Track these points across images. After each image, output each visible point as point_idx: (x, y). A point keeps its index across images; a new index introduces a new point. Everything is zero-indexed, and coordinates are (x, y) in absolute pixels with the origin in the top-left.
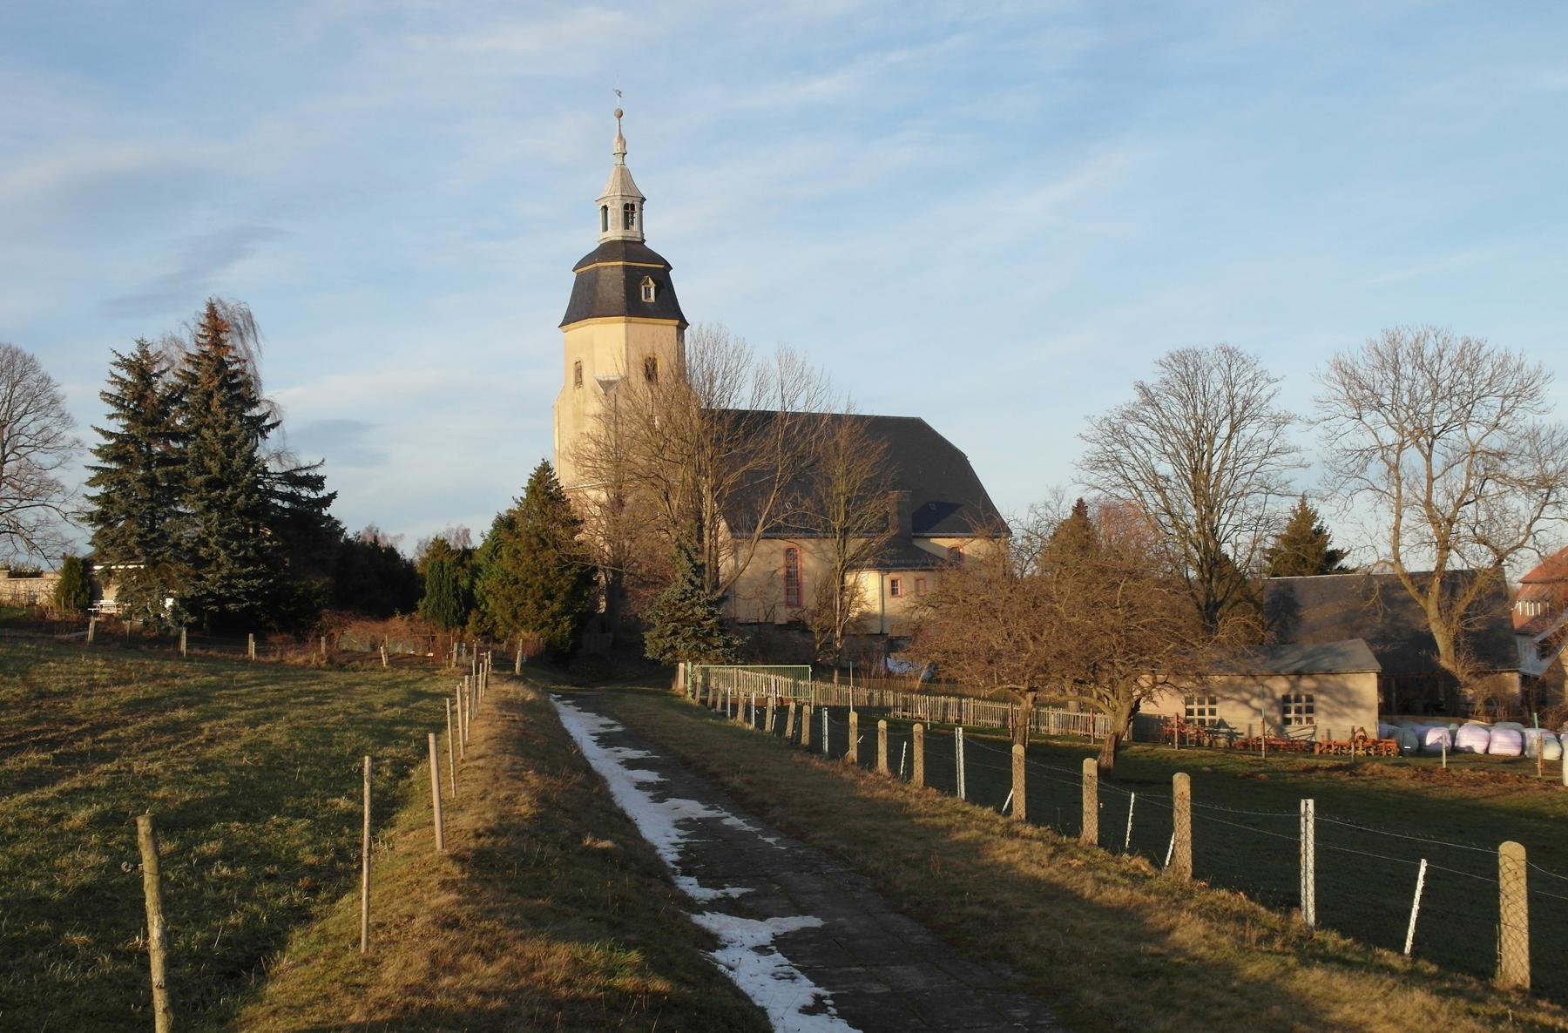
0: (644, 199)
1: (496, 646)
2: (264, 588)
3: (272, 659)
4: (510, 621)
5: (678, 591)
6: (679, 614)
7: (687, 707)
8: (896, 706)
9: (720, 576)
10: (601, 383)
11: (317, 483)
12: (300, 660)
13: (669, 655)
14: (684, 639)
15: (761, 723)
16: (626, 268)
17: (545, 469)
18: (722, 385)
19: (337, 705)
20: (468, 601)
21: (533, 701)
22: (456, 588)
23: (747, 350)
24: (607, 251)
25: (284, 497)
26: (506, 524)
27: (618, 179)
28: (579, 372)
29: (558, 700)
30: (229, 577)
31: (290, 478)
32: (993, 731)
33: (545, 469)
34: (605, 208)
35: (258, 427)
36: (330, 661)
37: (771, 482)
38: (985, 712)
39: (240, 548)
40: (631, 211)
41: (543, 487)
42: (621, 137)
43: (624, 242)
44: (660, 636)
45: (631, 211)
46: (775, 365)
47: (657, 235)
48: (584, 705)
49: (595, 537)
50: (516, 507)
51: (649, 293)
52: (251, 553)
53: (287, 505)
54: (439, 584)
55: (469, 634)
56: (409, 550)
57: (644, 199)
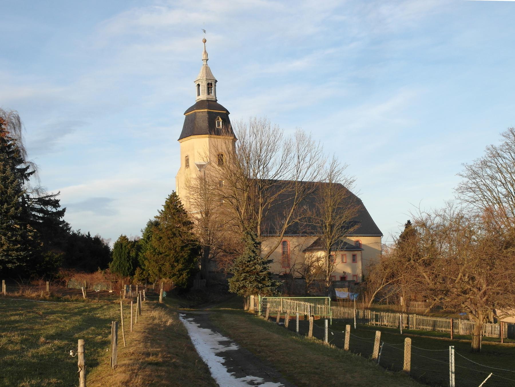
0: (216, 81)
1: (149, 286)
2: (27, 257)
3: (16, 294)
4: (158, 273)
5: (247, 256)
6: (248, 268)
7: (262, 323)
8: (372, 319)
9: (245, 255)
10: (198, 165)
11: (56, 204)
12: (34, 295)
13: (242, 291)
14: (250, 282)
15: (337, 339)
17: (174, 196)
18: (267, 149)
20: (136, 264)
21: (172, 325)
22: (129, 257)
23: (281, 130)
24: (200, 105)
25: (41, 211)
26: (153, 226)
27: (205, 71)
28: (187, 161)
29: (184, 318)
30: (8, 250)
31: (42, 201)
32: (428, 333)
33: (174, 196)
34: (199, 85)
35: (23, 175)
36: (52, 295)
37: (292, 201)
38: (423, 322)
39: (13, 235)
40: (210, 86)
41: (173, 204)
42: (205, 52)
43: (208, 101)
44: (237, 281)
45: (210, 86)
46: (294, 140)
48: (203, 323)
49: (197, 231)
50: (158, 215)
51: (220, 123)
52: (19, 238)
53: (41, 215)
54: (120, 255)
55: (135, 280)
57: (216, 81)
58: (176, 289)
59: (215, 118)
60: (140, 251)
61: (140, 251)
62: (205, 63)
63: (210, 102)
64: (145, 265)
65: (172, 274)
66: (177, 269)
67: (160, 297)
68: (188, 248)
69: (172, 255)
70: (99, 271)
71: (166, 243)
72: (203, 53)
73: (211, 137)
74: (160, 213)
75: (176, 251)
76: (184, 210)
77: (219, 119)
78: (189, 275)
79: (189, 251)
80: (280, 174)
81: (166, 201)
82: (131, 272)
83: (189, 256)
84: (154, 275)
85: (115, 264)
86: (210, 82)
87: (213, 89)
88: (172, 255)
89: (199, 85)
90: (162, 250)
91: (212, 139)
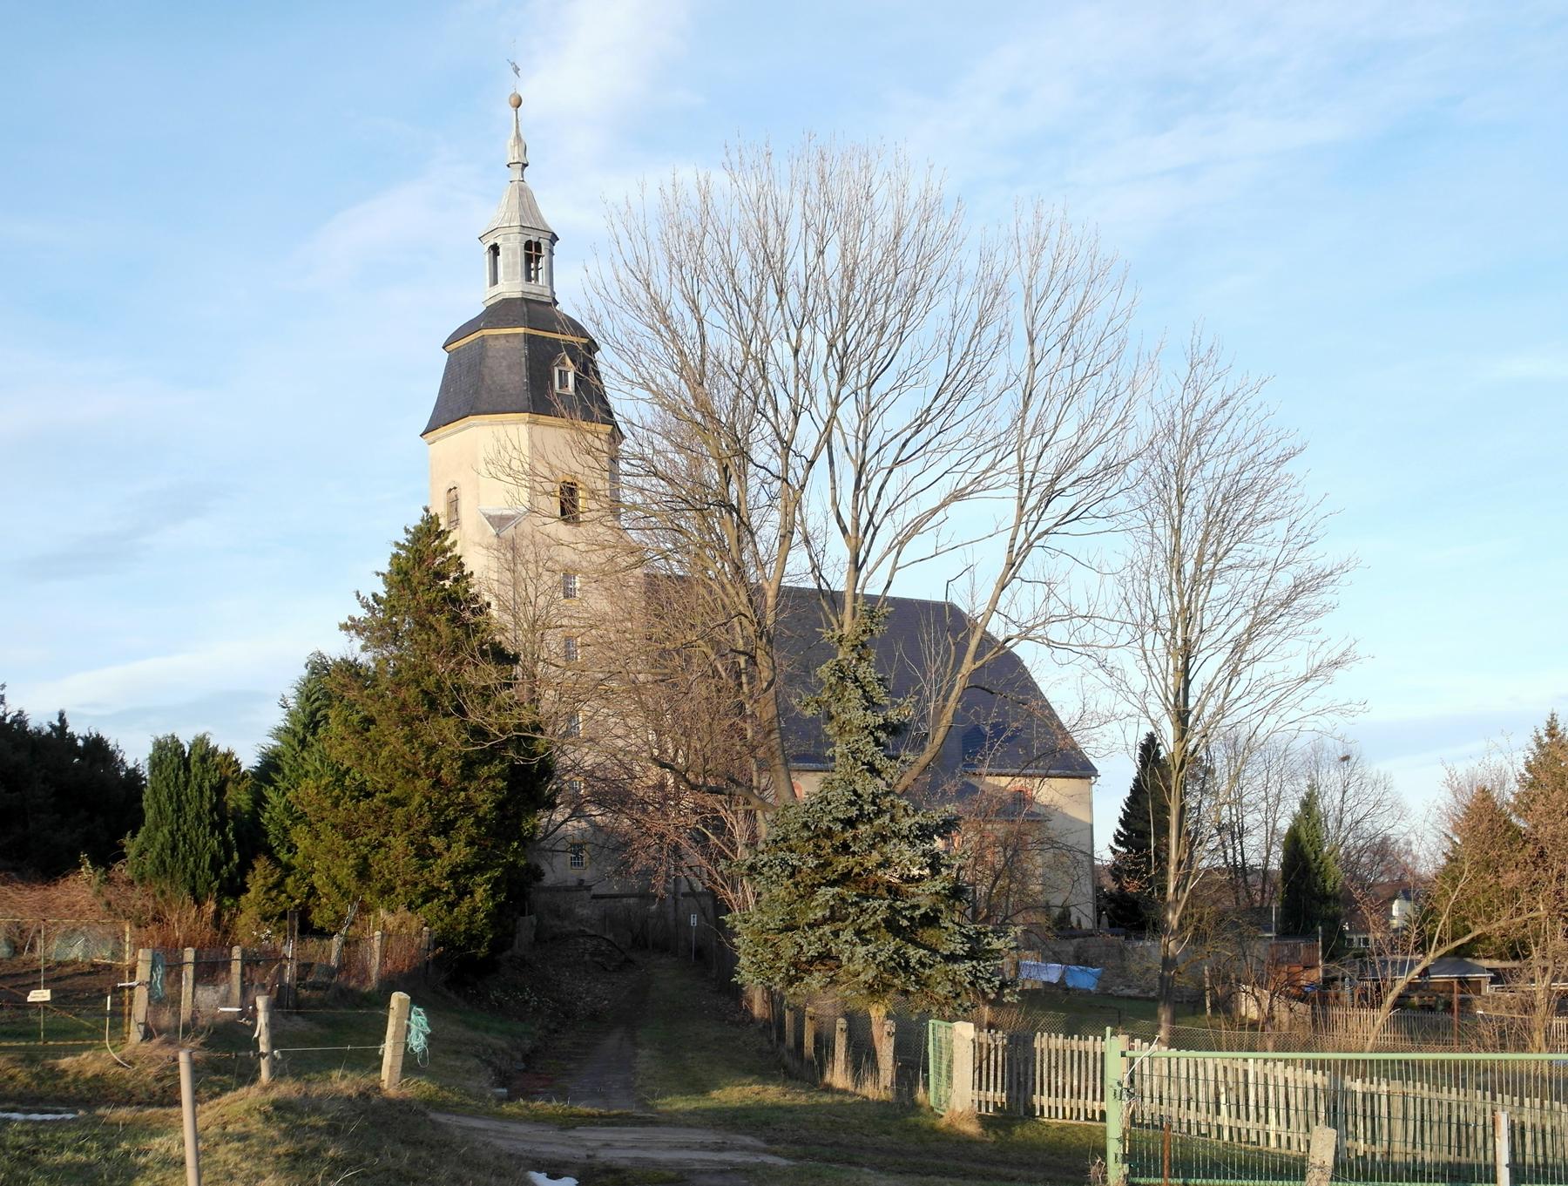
10: (490, 518)
16: (529, 339)
19: (1163, 604)
27: (516, 201)
34: (495, 249)
41: (424, 576)
47: (574, 289)
51: (566, 378)
56: (135, 752)
58: (438, 958)
59: (553, 358)
60: (271, 782)
61: (271, 782)
62: (517, 176)
63: (533, 306)
64: (292, 849)
65: (421, 888)
66: (441, 866)
67: (389, 1051)
68: (496, 767)
69: (417, 799)
70: (86, 870)
71: (394, 737)
72: (511, 141)
73: (535, 423)
74: (366, 606)
75: (438, 783)
76: (475, 598)
77: (564, 364)
78: (502, 898)
79: (501, 784)
80: (938, 423)
81: (396, 556)
82: (231, 879)
83: (500, 806)
84: (336, 896)
85: (150, 839)
86: (534, 238)
87: (543, 263)
88: (417, 799)
89: (495, 249)
90: (373, 779)
91: (537, 429)
